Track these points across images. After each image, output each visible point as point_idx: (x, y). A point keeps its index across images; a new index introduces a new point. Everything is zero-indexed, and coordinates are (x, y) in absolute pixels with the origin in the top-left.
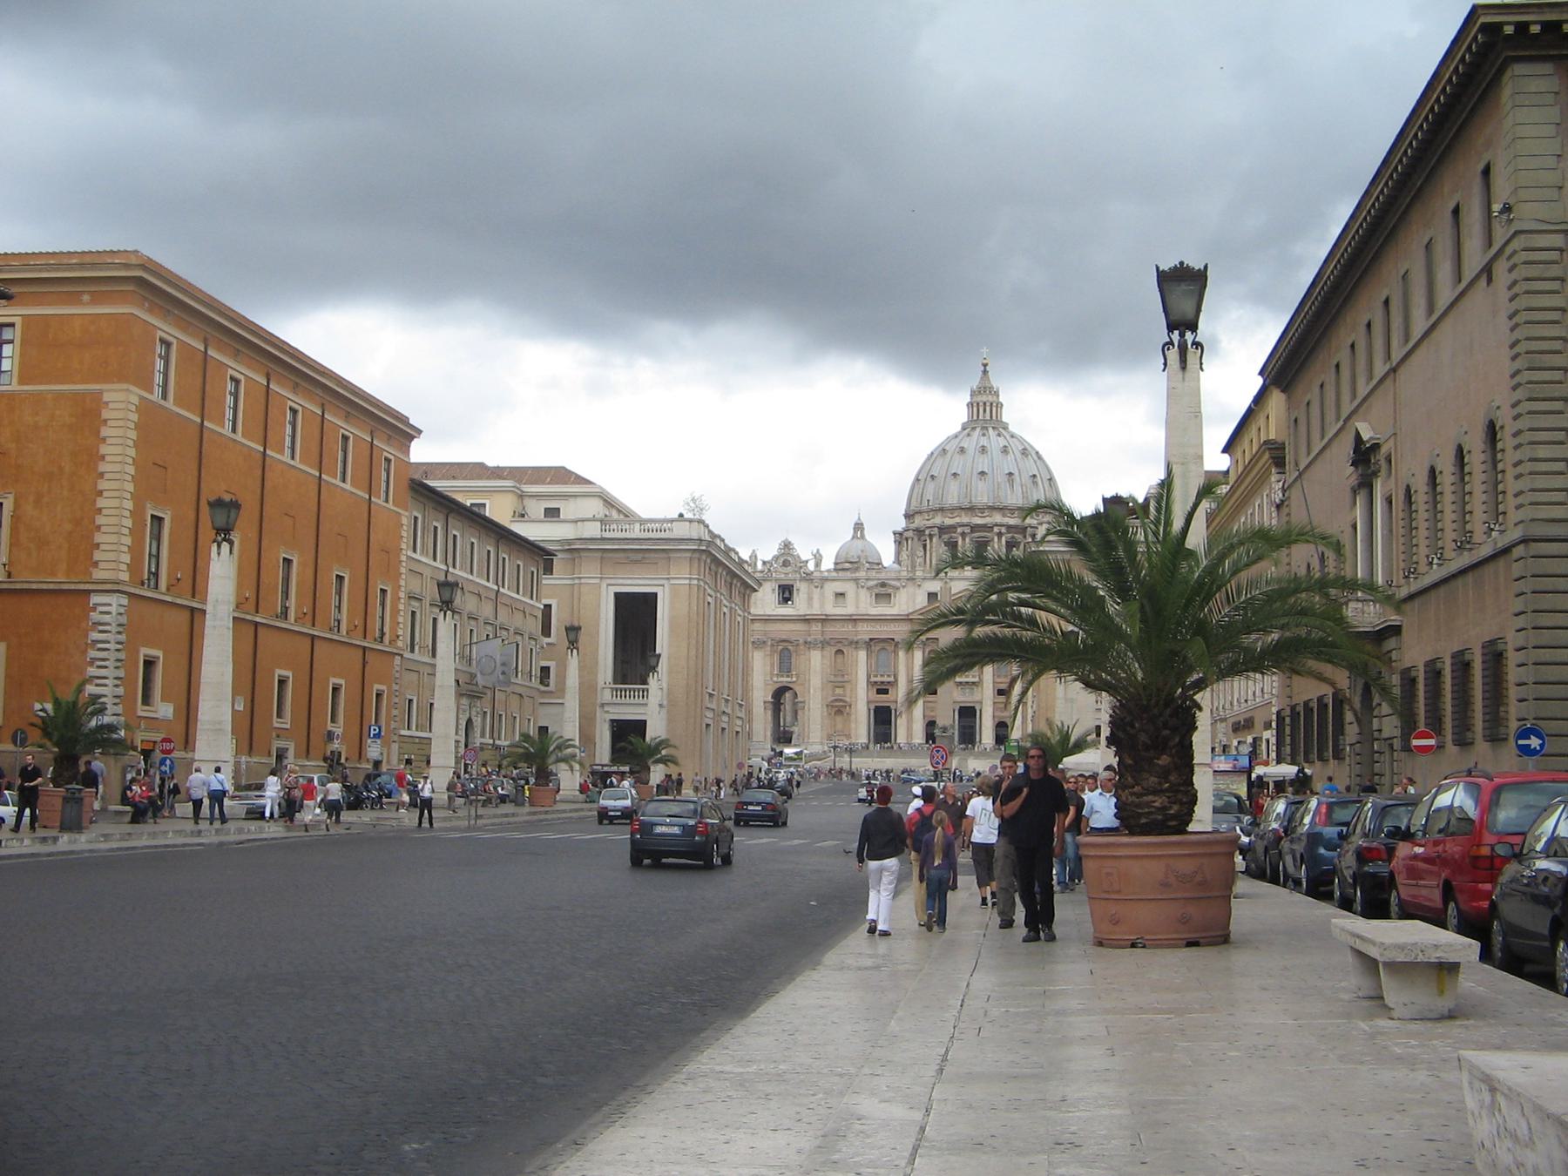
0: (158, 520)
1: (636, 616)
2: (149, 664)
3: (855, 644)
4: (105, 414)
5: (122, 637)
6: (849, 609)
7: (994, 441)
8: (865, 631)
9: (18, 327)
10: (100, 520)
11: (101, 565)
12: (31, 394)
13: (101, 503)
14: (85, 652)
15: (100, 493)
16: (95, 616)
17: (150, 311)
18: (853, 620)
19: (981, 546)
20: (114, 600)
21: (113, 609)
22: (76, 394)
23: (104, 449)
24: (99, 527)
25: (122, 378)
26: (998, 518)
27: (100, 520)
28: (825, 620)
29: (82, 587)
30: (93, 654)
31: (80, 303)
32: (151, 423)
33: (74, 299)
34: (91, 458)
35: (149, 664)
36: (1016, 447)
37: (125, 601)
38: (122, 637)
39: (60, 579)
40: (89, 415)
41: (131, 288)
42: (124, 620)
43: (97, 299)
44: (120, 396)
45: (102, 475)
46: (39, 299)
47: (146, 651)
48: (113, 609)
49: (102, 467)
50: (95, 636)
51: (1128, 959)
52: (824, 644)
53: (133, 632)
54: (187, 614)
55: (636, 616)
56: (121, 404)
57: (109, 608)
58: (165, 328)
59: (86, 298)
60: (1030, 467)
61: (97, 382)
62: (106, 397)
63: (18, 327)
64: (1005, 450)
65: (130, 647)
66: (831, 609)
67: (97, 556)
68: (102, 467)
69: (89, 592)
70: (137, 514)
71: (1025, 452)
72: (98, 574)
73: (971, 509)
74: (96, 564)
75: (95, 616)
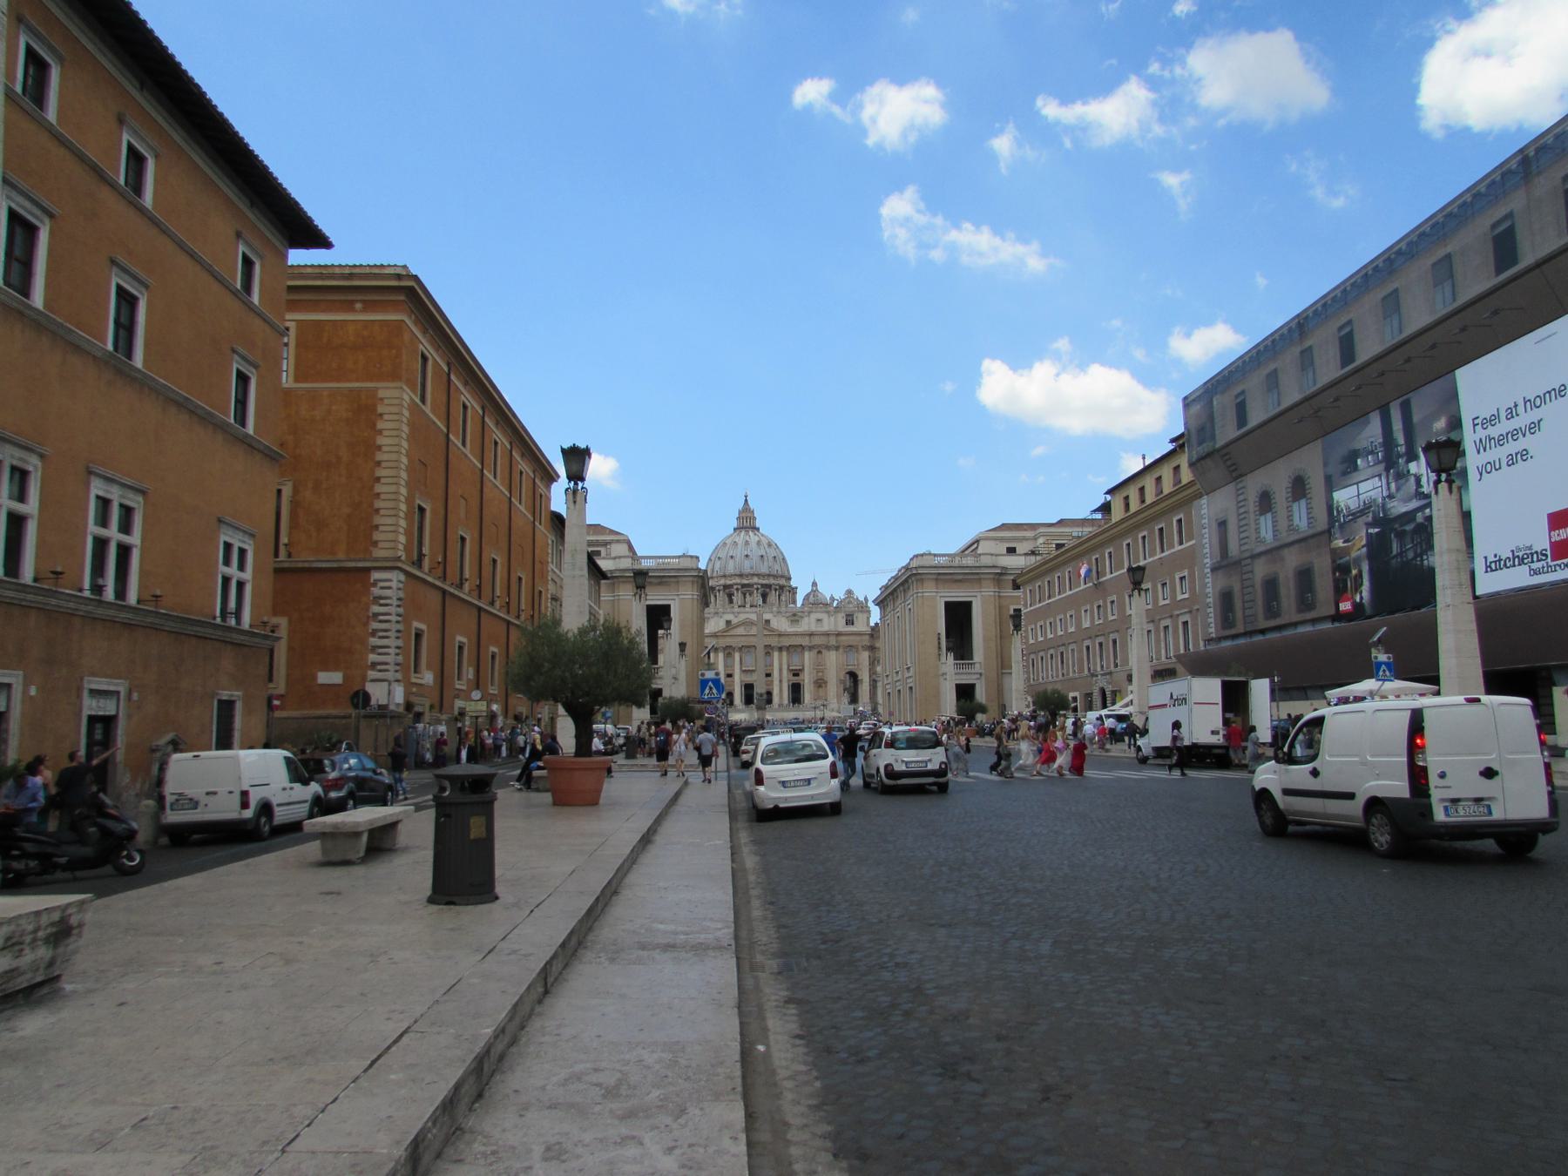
0: (422, 510)
1: (958, 616)
2: (418, 636)
3: (828, 648)
4: (380, 409)
5: (401, 610)
6: (825, 627)
7: (753, 537)
8: (786, 642)
9: (293, 333)
10: (378, 504)
11: (380, 545)
12: (308, 390)
13: (378, 488)
14: (366, 624)
15: (378, 479)
16: (376, 591)
17: (415, 323)
18: (827, 634)
19: (764, 596)
20: (395, 578)
21: (394, 584)
22: (351, 390)
23: (380, 441)
24: (377, 511)
25: (394, 376)
26: (755, 580)
27: (378, 504)
28: (811, 635)
29: (360, 565)
30: (375, 625)
31: (353, 310)
32: (419, 428)
33: (349, 306)
34: (370, 448)
35: (418, 636)
36: (765, 542)
37: (402, 577)
38: (401, 610)
39: (342, 558)
40: (365, 412)
41: (402, 298)
42: (401, 594)
43: (369, 306)
44: (396, 393)
45: (379, 463)
46: (314, 306)
47: (416, 624)
48: (394, 584)
49: (379, 456)
50: (376, 609)
51: (767, 825)
52: (811, 648)
53: (411, 606)
54: (438, 597)
55: (958, 616)
56: (396, 400)
57: (390, 584)
58: (426, 346)
59: (358, 306)
60: (772, 553)
61: (371, 380)
62: (381, 394)
63: (293, 333)
64: (759, 543)
65: (405, 619)
66: (814, 628)
67: (377, 536)
68: (379, 456)
69: (368, 570)
70: (409, 500)
71: (770, 545)
72: (378, 553)
73: (741, 576)
74: (375, 544)
75: (376, 591)
